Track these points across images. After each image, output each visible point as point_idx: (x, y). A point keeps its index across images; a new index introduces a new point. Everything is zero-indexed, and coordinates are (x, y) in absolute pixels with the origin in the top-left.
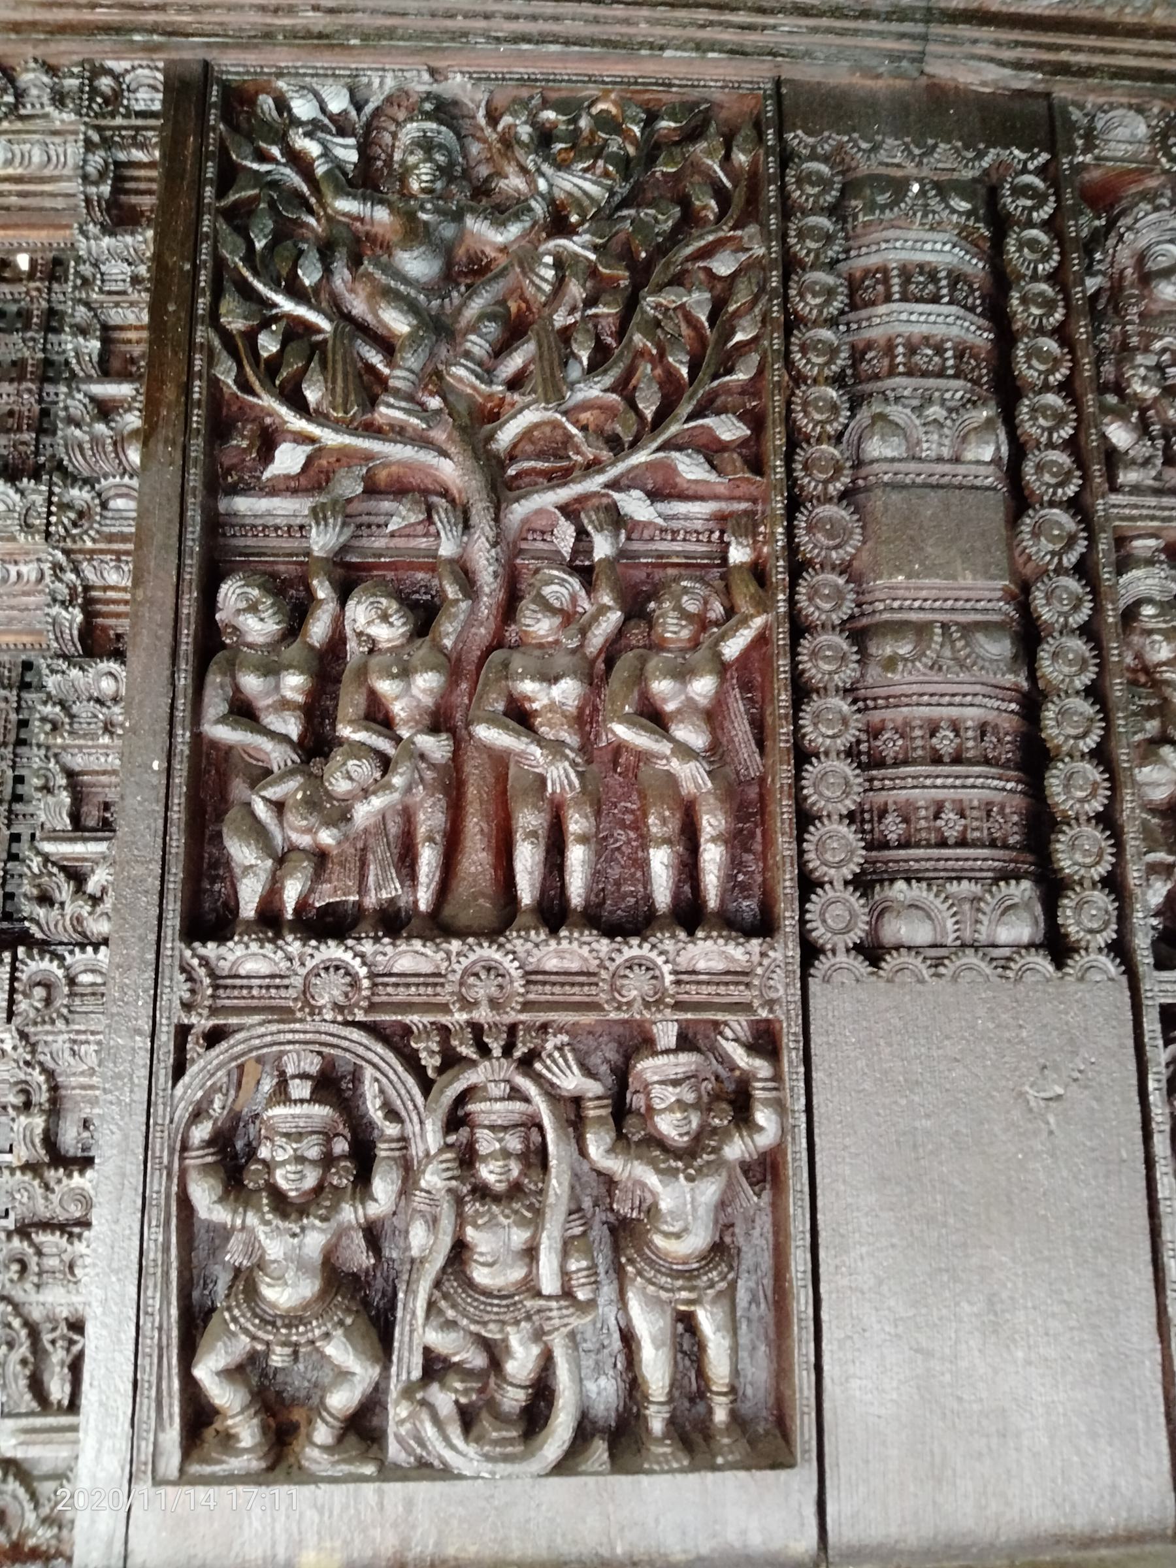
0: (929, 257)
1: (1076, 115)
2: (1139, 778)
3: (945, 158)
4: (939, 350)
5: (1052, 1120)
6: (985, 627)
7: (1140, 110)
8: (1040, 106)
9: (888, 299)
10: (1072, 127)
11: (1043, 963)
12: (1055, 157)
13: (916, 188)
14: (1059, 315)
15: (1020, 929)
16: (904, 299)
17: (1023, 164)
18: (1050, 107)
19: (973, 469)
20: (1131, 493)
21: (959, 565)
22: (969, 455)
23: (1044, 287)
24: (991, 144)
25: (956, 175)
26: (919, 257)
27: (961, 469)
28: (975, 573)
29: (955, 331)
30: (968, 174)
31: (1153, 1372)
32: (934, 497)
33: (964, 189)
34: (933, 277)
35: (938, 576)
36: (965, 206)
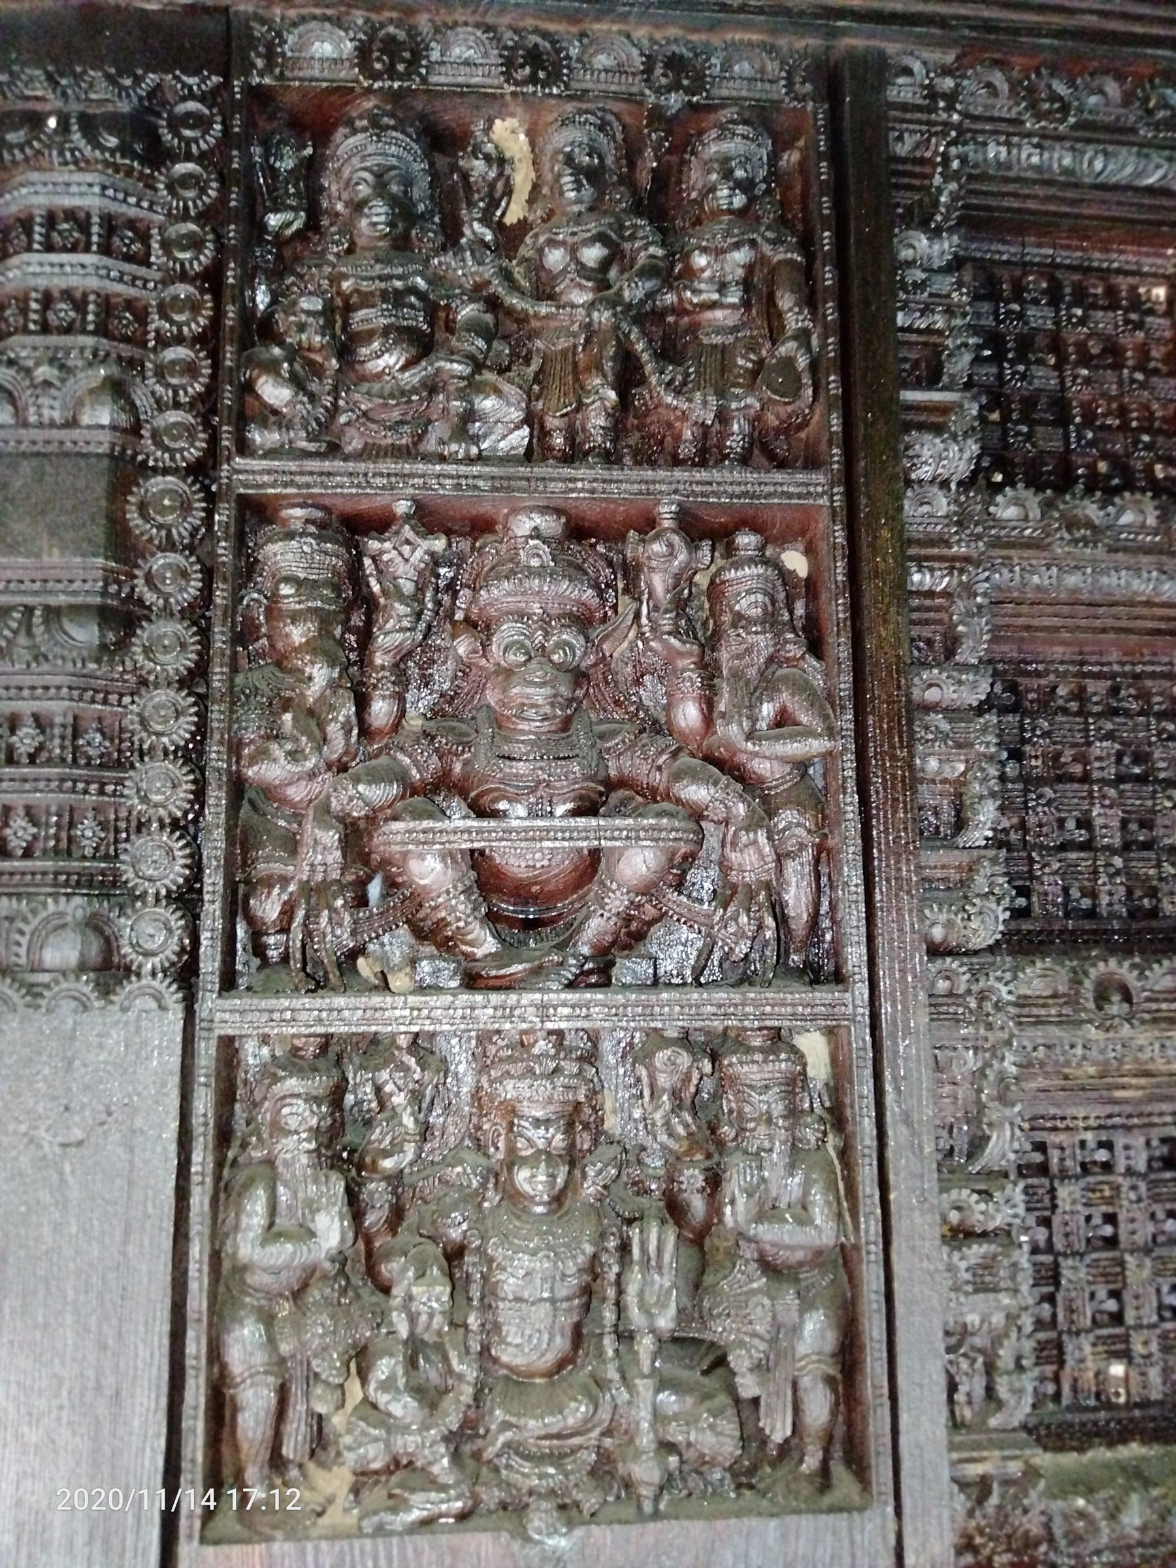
0: (76, 202)
1: (259, 30)
2: (970, 442)
3: (100, 92)
4: (80, 305)
5: (67, 1168)
6: (76, 610)
7: (337, 22)
8: (211, 25)
9: (29, 249)
10: (251, 42)
11: (85, 985)
12: (227, 77)
13: (52, 123)
14: (207, 255)
15: (63, 951)
16: (49, 247)
17: (187, 93)
18: (228, 24)
19: (40, 435)
20: (264, 456)
21: (44, 542)
22: (86, 420)
23: (192, 227)
24: (149, 68)
25: (110, 108)
26: (68, 202)
27: (76, 434)
28: (63, 550)
29: (93, 283)
30: (124, 107)
31: (153, 1459)
32: (26, 467)
33: (114, 123)
34: (84, 225)
35: (19, 553)
36: (113, 142)
